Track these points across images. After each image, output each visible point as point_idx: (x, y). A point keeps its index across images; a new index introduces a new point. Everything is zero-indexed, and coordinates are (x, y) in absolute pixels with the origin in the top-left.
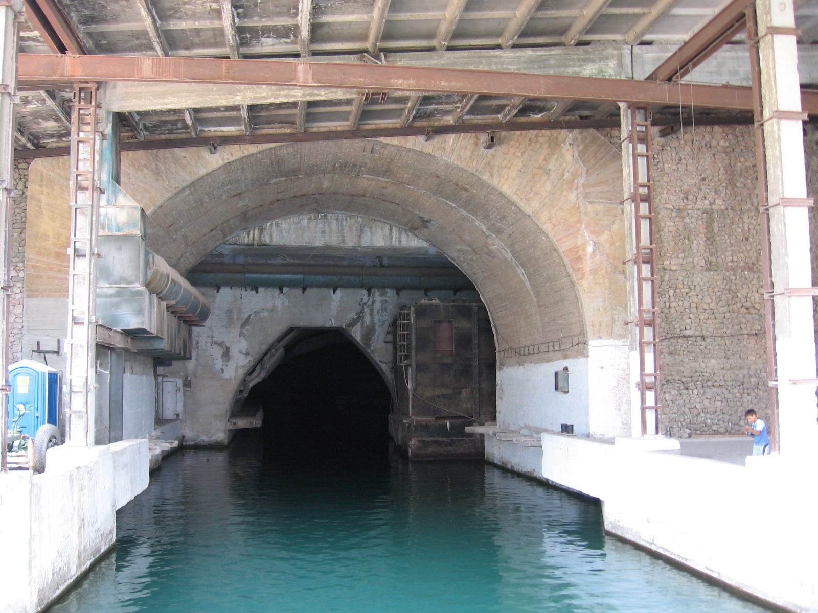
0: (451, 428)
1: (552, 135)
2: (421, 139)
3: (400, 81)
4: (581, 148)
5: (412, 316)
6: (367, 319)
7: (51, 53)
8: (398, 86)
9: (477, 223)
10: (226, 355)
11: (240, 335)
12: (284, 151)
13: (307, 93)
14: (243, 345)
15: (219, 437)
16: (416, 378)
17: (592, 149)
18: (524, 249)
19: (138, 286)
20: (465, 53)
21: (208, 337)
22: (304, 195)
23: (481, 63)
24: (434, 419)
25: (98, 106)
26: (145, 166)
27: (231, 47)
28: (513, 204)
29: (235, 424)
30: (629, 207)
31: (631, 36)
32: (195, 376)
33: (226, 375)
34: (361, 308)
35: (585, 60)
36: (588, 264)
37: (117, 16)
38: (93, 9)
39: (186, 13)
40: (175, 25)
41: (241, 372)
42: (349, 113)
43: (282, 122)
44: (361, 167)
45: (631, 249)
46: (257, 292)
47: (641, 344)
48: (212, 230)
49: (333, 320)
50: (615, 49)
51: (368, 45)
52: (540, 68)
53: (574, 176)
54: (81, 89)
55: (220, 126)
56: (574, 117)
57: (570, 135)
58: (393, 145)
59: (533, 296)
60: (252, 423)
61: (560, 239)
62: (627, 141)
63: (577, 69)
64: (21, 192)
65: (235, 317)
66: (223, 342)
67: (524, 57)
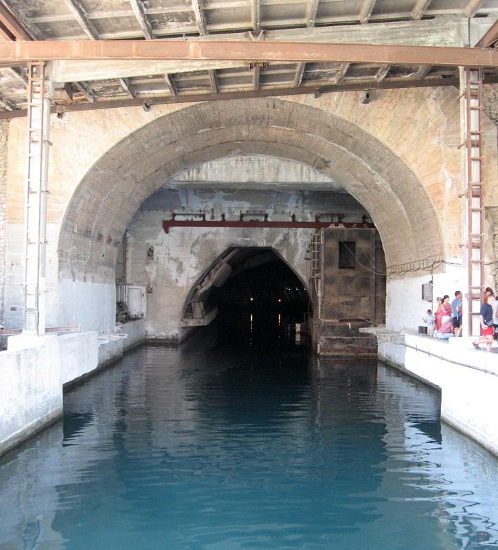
0: (353, 328)
1: (419, 92)
2: (311, 96)
4: (442, 102)
5: (322, 238)
7: (6, 41)
9: (364, 163)
10: (180, 269)
11: (191, 253)
12: (203, 109)
16: (324, 288)
17: (452, 102)
18: (399, 185)
20: (331, 28)
22: (228, 142)
23: (343, 36)
25: (46, 79)
26: (95, 122)
27: (144, 30)
28: (387, 148)
29: (187, 322)
30: (464, 151)
31: (467, 10)
32: (156, 285)
33: (180, 284)
35: (429, 31)
36: (447, 196)
37: (54, 11)
38: (35, 6)
39: (105, 6)
40: (96, 15)
41: (192, 282)
42: (251, 76)
43: (199, 86)
44: (269, 119)
45: (465, 185)
47: (470, 263)
48: (157, 171)
50: (455, 21)
51: (251, 25)
52: (392, 38)
53: (437, 125)
54: (33, 66)
55: (151, 89)
56: (436, 76)
57: (434, 91)
58: (288, 102)
59: (409, 222)
60: (200, 322)
61: (424, 177)
62: (464, 96)
63: (423, 39)
64: (4, 144)
66: (177, 258)
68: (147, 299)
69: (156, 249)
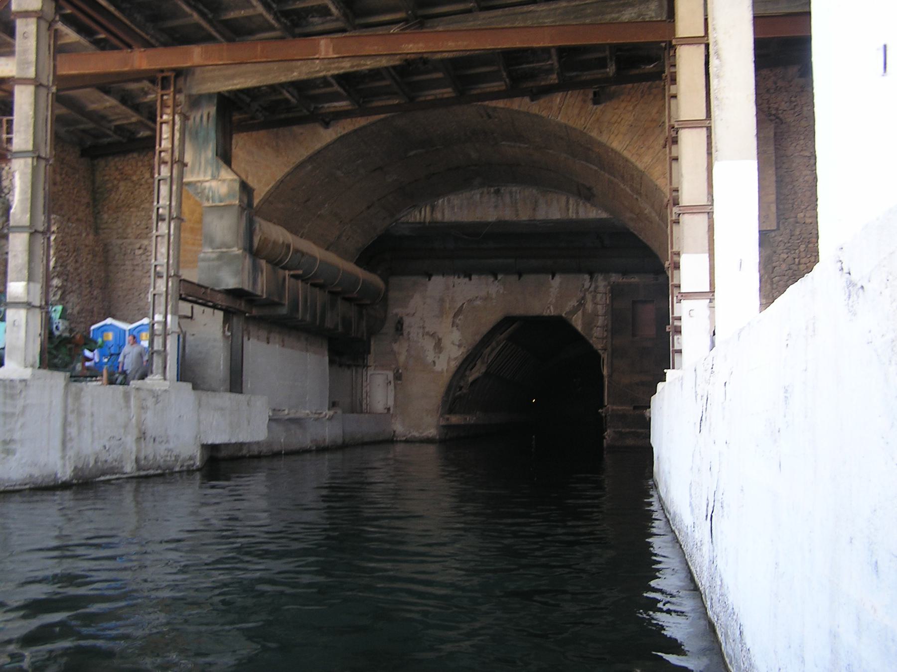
2: (527, 99)
3: (411, 46)
6: (589, 306)
8: (408, 50)
10: (439, 346)
11: (453, 326)
13: (355, 64)
14: (456, 336)
15: (430, 433)
19: (236, 251)
21: (420, 327)
24: (632, 408)
29: (448, 419)
33: (438, 368)
34: (582, 295)
41: (454, 365)
46: (470, 279)
48: (369, 208)
49: (552, 308)
60: (466, 419)
63: (615, 15)
65: (448, 306)
67: (559, 8)
68: (395, 387)
69: (407, 321)
